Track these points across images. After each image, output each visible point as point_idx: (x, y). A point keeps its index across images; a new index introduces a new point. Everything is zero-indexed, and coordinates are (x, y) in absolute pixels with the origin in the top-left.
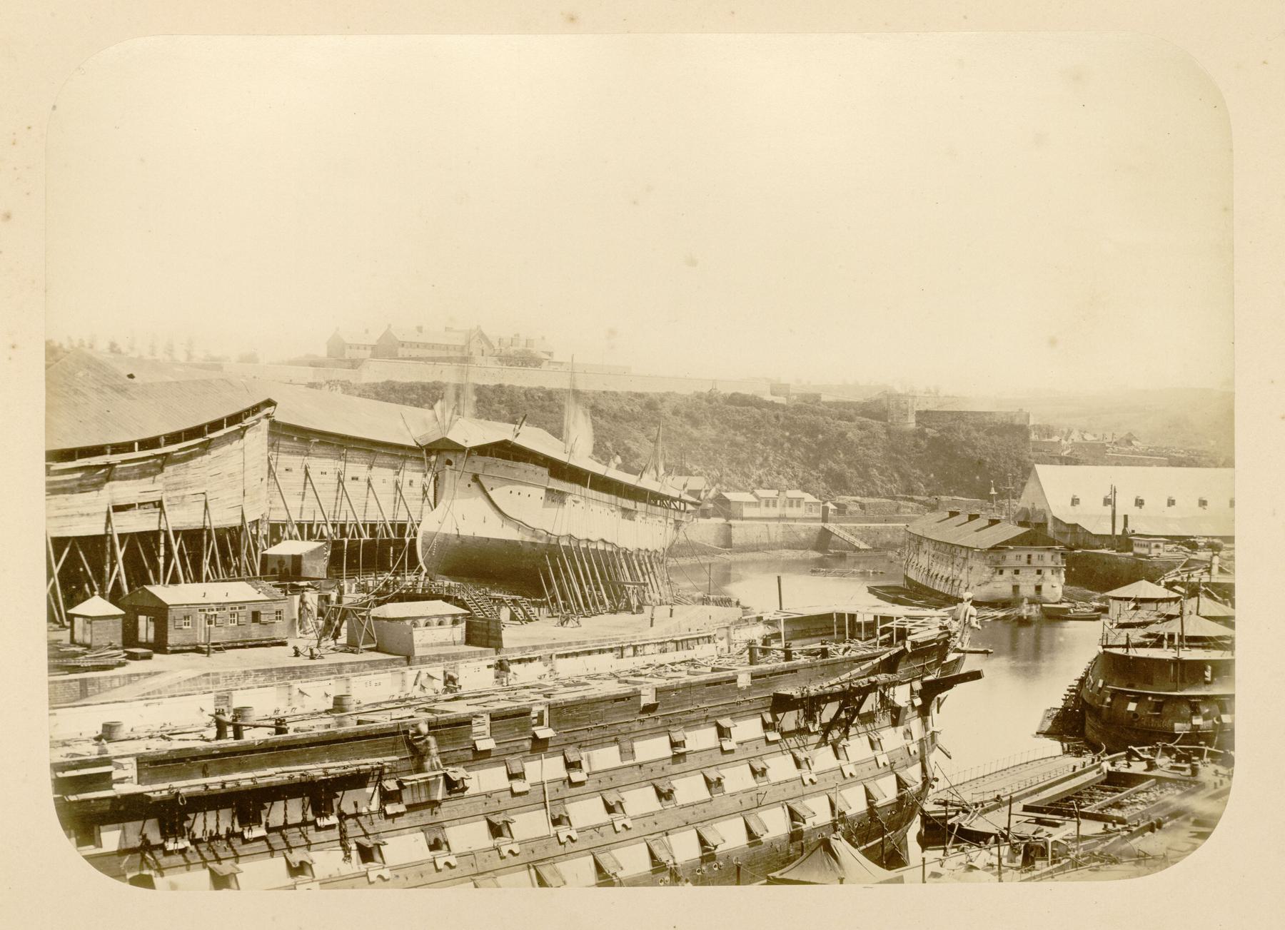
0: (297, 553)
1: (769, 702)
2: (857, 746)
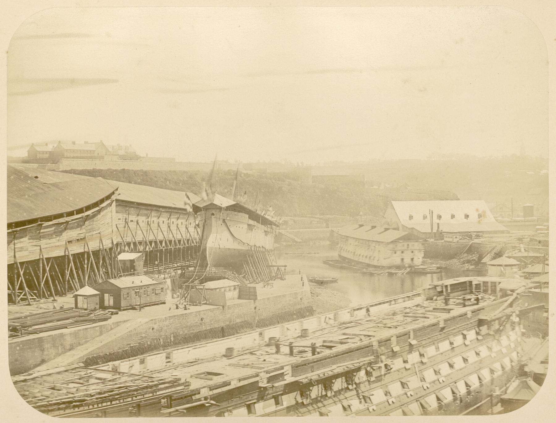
0: (132, 259)
1: (476, 323)
2: (504, 340)
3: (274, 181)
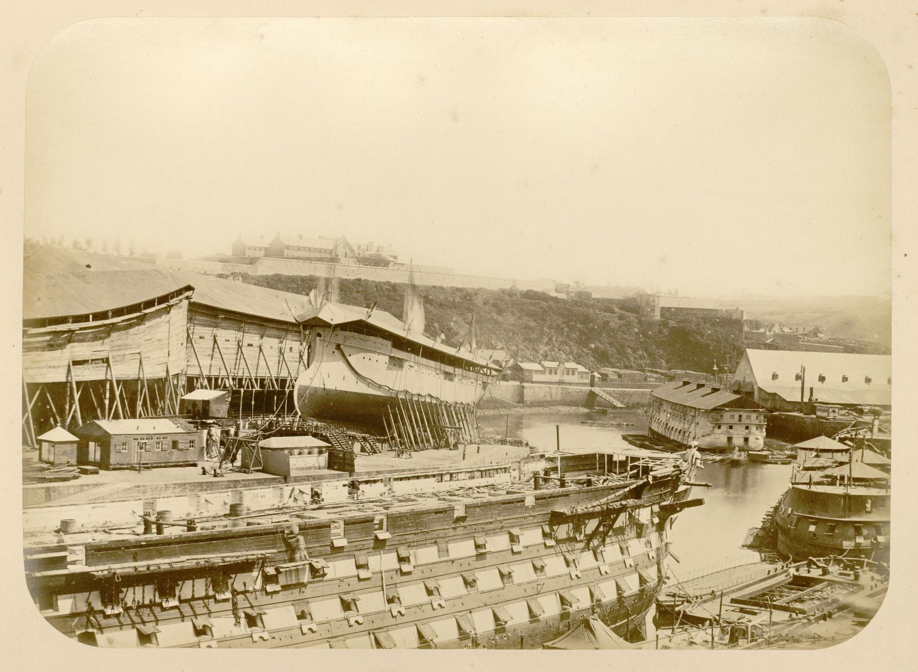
0: (206, 399)
2: (611, 551)
3: (598, 312)
